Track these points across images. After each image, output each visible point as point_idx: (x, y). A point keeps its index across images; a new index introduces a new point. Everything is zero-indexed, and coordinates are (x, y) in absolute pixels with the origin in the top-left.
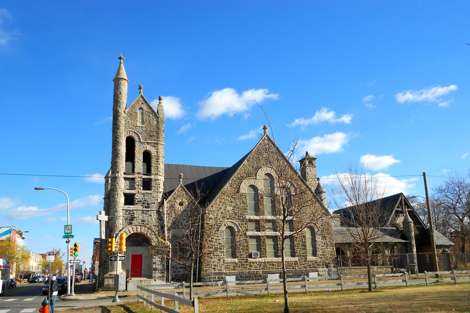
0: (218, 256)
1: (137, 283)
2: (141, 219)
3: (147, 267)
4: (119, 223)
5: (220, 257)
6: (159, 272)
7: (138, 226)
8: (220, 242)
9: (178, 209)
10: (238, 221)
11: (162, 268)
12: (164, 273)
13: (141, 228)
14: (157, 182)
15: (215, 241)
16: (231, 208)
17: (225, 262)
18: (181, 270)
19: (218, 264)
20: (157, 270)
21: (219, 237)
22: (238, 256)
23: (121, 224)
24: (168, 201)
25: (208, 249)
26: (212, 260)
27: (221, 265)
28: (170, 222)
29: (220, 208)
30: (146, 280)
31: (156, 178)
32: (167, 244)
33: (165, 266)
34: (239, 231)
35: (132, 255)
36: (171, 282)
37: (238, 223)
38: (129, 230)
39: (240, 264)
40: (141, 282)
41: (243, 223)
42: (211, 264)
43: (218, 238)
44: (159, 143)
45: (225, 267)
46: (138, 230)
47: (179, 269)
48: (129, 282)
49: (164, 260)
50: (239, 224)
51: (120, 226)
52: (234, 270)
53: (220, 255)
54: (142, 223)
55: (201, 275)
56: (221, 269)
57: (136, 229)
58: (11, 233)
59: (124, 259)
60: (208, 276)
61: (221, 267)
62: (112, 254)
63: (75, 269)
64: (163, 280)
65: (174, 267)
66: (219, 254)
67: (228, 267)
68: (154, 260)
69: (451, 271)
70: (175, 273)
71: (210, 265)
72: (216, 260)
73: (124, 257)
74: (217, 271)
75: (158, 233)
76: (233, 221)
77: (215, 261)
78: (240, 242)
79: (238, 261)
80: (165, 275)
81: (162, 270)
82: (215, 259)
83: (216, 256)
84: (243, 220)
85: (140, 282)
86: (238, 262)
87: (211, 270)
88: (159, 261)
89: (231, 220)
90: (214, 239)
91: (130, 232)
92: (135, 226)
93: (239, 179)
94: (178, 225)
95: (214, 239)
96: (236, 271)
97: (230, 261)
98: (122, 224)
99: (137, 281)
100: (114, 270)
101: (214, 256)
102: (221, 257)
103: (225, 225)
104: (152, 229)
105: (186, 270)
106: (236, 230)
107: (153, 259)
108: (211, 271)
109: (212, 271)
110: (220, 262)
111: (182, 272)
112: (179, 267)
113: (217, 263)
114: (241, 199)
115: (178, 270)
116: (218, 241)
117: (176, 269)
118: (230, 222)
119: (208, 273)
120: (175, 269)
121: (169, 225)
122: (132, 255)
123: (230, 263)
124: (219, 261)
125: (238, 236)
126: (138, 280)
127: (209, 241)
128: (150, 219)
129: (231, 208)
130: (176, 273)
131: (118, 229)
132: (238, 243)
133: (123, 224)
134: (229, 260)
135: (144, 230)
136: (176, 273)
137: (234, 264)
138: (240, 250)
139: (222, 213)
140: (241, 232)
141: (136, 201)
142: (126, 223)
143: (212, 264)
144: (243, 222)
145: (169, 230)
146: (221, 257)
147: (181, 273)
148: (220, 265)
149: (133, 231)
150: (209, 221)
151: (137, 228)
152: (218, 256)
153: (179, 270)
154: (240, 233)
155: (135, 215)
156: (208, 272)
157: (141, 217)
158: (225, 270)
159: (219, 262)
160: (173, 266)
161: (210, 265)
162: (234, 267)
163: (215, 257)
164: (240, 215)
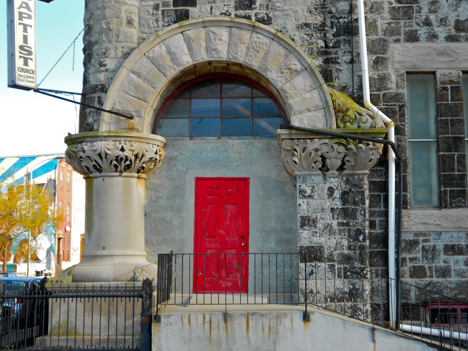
1: (207, 326)
3: (272, 245)
4: (124, 16)
7: (214, 29)
11: (349, 248)
12: (360, 275)
13: (231, 35)
18: (452, 264)
20: (320, 261)
23: (130, 22)
30: (253, 314)
32: (372, 118)
33: (364, 240)
35: (199, 181)
36: (405, 327)
38: (169, 52)
40: (225, 320)
46: (215, 50)
47: (443, 257)
48: (163, 320)
49: (359, 208)
51: (125, 28)
54: (242, 12)
57: (204, 44)
58: (55, 168)
62: (92, 169)
64: (354, 313)
65: (416, 243)
68: (304, 206)
80: (368, 287)
81: (347, 259)
85: (222, 324)
88: (332, 209)
91: (174, 58)
92: (203, 31)
94: (427, 23)
98: (136, 23)
99: (207, 319)
100: (105, 252)
104: (290, 42)
107: (300, 201)
112: (440, 246)
115: (440, 262)
117: (425, 257)
120: (419, 255)
122: (199, 181)
126: (211, 313)
131: (119, 45)
133: (143, 22)
135: (248, 48)
136: (428, 280)
141: (404, 193)
142: (160, 18)
147: (454, 279)
149: (192, 55)
151: (212, 36)
153: (442, 264)
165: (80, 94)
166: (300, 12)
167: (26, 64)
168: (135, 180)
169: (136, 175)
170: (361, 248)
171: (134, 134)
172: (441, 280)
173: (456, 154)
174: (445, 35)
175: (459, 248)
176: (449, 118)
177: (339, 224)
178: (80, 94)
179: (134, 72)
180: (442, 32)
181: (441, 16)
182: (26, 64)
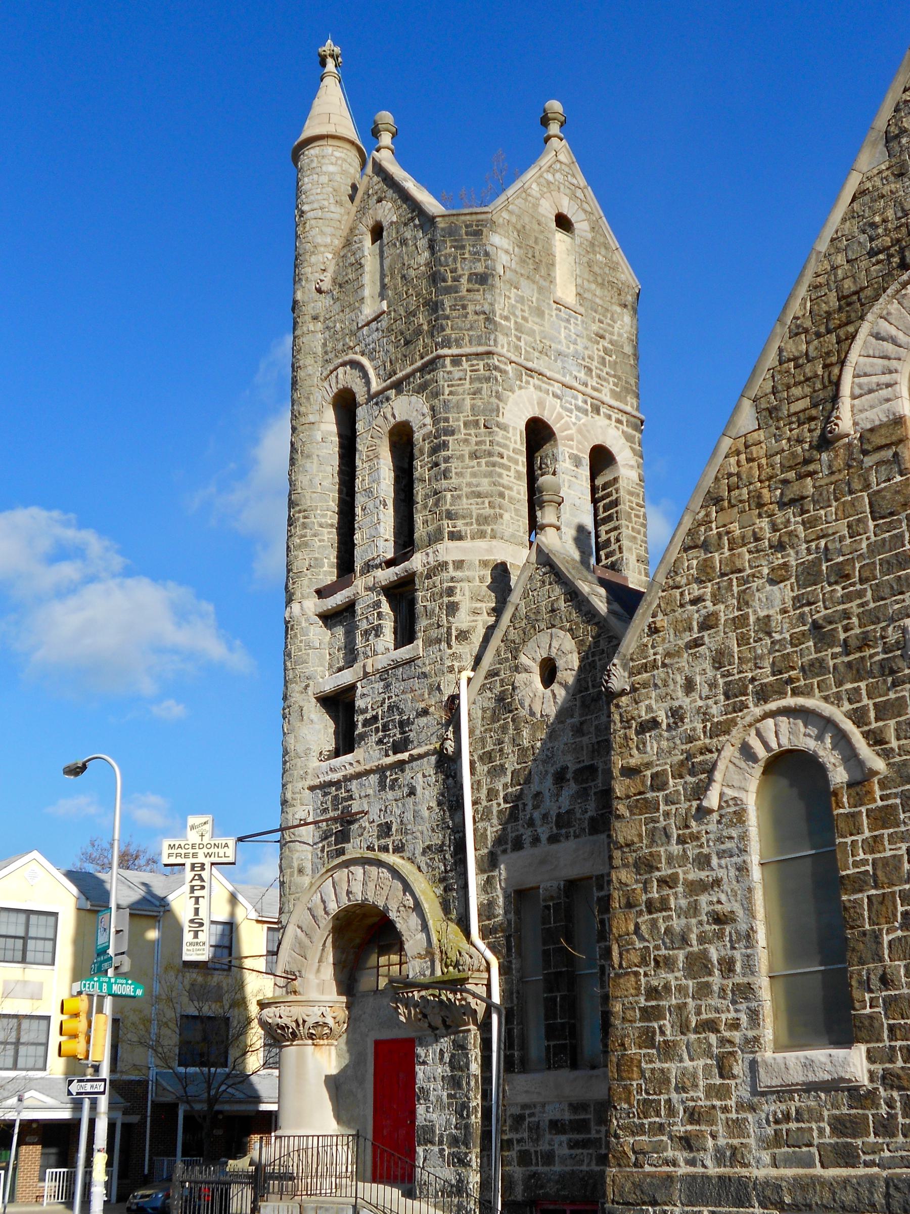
0: (711, 1026)
2: (375, 824)
4: (295, 864)
5: (723, 1041)
6: (443, 1156)
8: (719, 902)
9: (532, 714)
10: (849, 686)
14: (438, 583)
15: (683, 902)
16: (784, 593)
17: (766, 1080)
19: (718, 1103)
20: (432, 1143)
21: (715, 861)
22: (871, 1017)
23: (301, 871)
24: (486, 678)
25: (646, 975)
26: (673, 1067)
27: (740, 1107)
28: (495, 809)
29: (707, 624)
31: (431, 559)
34: (859, 783)
35: (377, 1043)
37: (847, 706)
39: (890, 1104)
41: (892, 695)
42: (669, 1101)
43: (703, 875)
44: (439, 357)
45: (770, 1131)
47: (548, 1136)
50: (858, 717)
51: (297, 878)
52: (847, 1157)
53: (724, 1017)
55: (604, 1195)
56: (734, 1149)
59: (102, 1090)
60: (644, 1203)
61: (737, 1127)
63: (10, 1149)
66: (717, 1010)
67: (793, 1125)
69: (610, 611)
70: (525, 1166)
71: (658, 1115)
72: (701, 1063)
73: (103, 1083)
74: (708, 1163)
75: (445, 890)
76: (800, 701)
77: (694, 1076)
78: (876, 887)
79: (871, 1073)
82: (692, 1059)
83: (696, 1032)
84: (892, 672)
86: (872, 1076)
87: (669, 1154)
89: (790, 701)
90: (680, 889)
93: (829, 332)
95: (680, 889)
96: (861, 1171)
97: (797, 1076)
101: (682, 1033)
102: (736, 1036)
103: (747, 752)
105: (584, 1144)
106: (839, 776)
108: (667, 1162)
109: (674, 1163)
110: (732, 1082)
111: (563, 1160)
113: (711, 1091)
114: (856, 485)
116: (703, 899)
118: (783, 720)
119: (649, 1174)
120: (526, 1135)
121: (492, 829)
122: (377, 1043)
123: (810, 1088)
124: (722, 1076)
125: (859, 832)
127: (650, 905)
128: (409, 816)
129: (784, 593)
130: (533, 1168)
132: (863, 896)
134: (791, 1064)
136: (533, 1168)
137: (843, 1097)
138: (881, 959)
139: (719, 659)
140: (883, 785)
143: (674, 1096)
144: (894, 685)
145: (489, 863)
146: (736, 1036)
147: (557, 1168)
148: (725, 1109)
150: (638, 748)
152: (711, 1026)
154: (870, 792)
155: (355, 807)
156: (647, 1168)
157: (374, 814)
158: (766, 1157)
159: (718, 1081)
160: (517, 1111)
161: (658, 1115)
162: (840, 1126)
163: (693, 1037)
164: (857, 631)
165: (246, 957)
166: (425, 832)
167: (196, 936)
168: (311, 1049)
169: (310, 1042)
170: (581, 1126)
171: (298, 998)
172: (546, 1169)
173: (558, 994)
174: (547, 836)
175: (562, 1125)
176: (551, 947)
177: (450, 1096)
178: (246, 957)
179: (299, 927)
180: (544, 832)
181: (543, 812)
182: (196, 936)
